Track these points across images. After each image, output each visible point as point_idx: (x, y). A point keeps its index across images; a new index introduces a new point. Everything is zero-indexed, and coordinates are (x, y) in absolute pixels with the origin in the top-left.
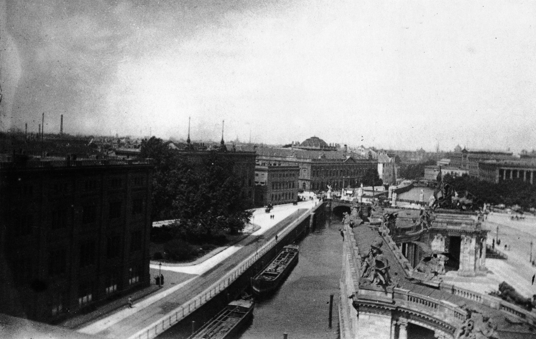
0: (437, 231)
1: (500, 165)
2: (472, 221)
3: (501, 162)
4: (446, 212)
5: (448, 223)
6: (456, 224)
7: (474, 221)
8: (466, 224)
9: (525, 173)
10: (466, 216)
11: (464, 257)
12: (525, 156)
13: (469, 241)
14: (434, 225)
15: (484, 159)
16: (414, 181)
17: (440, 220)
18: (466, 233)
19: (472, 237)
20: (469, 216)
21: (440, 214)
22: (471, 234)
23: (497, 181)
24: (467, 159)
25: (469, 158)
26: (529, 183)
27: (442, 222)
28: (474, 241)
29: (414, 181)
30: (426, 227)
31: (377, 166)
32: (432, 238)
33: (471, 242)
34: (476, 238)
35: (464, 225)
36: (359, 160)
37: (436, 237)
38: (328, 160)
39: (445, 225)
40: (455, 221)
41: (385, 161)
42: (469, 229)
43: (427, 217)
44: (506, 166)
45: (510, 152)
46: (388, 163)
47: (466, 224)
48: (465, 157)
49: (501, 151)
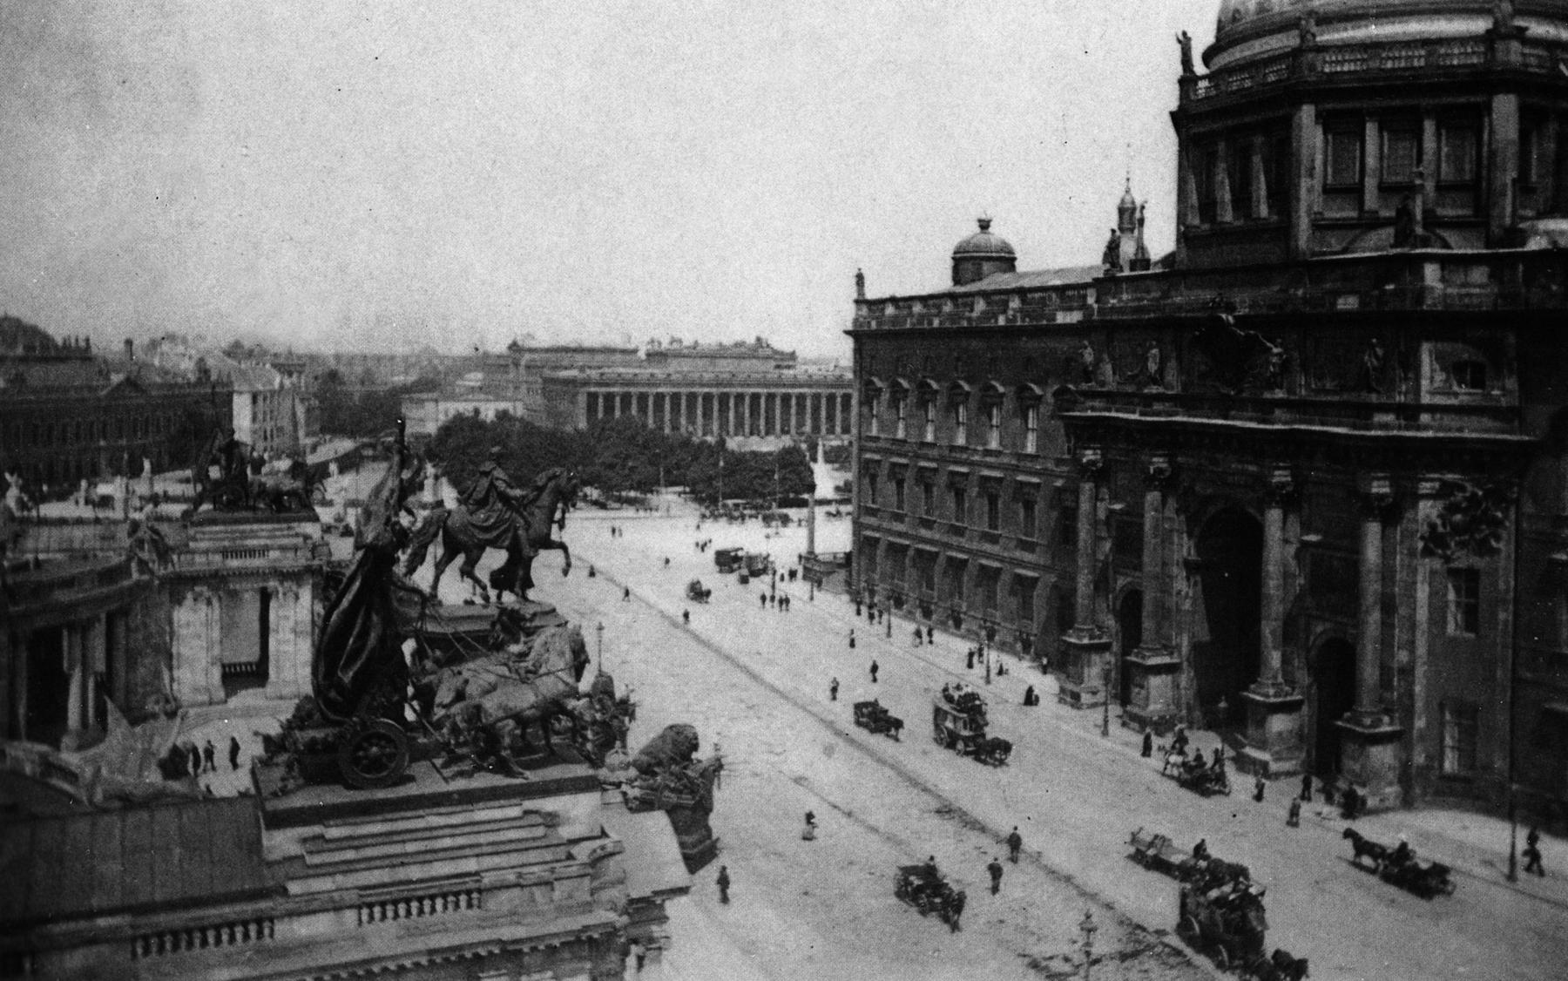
0: (193, 580)
1: (586, 383)
2: (301, 540)
3: (594, 374)
4: (224, 523)
5: (225, 553)
6: (251, 552)
7: (307, 537)
8: (283, 548)
9: (793, 402)
10: (284, 526)
11: (279, 642)
12: (657, 356)
13: (291, 595)
14: (179, 564)
15: (555, 368)
16: (366, 440)
17: (203, 545)
18: (283, 576)
19: (299, 586)
20: (295, 525)
21: (208, 529)
22: (296, 577)
23: (583, 425)
24: (522, 370)
25: (528, 367)
26: (645, 426)
27: (206, 552)
28: (306, 594)
29: (366, 440)
30: (151, 572)
31: (230, 402)
32: (178, 600)
33: (297, 597)
34: (314, 586)
35: (274, 554)
36: (161, 386)
37: (189, 596)
38: (35, 391)
39: (218, 558)
40: (251, 543)
41: (260, 387)
42: (290, 562)
43: (153, 541)
44: (702, 385)
45: (631, 346)
46: (273, 393)
47: (283, 548)
48: (517, 365)
49: (613, 346)
